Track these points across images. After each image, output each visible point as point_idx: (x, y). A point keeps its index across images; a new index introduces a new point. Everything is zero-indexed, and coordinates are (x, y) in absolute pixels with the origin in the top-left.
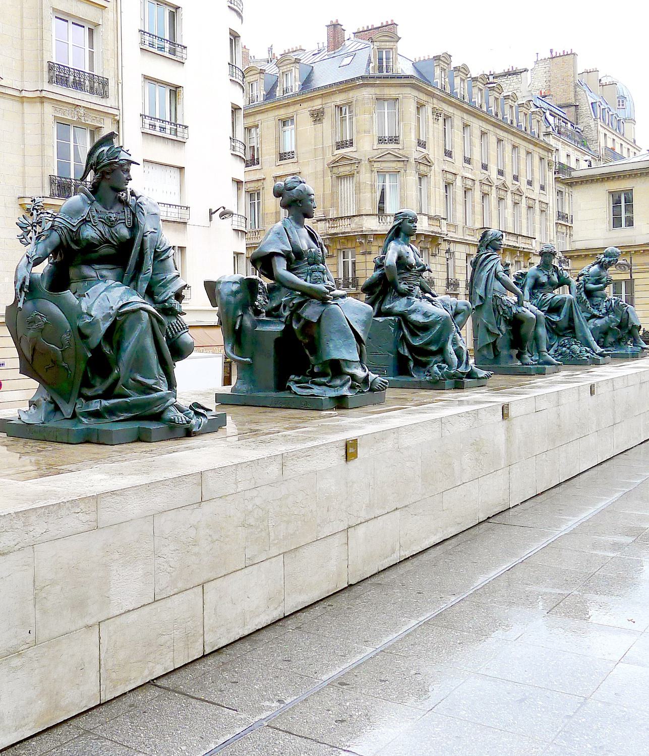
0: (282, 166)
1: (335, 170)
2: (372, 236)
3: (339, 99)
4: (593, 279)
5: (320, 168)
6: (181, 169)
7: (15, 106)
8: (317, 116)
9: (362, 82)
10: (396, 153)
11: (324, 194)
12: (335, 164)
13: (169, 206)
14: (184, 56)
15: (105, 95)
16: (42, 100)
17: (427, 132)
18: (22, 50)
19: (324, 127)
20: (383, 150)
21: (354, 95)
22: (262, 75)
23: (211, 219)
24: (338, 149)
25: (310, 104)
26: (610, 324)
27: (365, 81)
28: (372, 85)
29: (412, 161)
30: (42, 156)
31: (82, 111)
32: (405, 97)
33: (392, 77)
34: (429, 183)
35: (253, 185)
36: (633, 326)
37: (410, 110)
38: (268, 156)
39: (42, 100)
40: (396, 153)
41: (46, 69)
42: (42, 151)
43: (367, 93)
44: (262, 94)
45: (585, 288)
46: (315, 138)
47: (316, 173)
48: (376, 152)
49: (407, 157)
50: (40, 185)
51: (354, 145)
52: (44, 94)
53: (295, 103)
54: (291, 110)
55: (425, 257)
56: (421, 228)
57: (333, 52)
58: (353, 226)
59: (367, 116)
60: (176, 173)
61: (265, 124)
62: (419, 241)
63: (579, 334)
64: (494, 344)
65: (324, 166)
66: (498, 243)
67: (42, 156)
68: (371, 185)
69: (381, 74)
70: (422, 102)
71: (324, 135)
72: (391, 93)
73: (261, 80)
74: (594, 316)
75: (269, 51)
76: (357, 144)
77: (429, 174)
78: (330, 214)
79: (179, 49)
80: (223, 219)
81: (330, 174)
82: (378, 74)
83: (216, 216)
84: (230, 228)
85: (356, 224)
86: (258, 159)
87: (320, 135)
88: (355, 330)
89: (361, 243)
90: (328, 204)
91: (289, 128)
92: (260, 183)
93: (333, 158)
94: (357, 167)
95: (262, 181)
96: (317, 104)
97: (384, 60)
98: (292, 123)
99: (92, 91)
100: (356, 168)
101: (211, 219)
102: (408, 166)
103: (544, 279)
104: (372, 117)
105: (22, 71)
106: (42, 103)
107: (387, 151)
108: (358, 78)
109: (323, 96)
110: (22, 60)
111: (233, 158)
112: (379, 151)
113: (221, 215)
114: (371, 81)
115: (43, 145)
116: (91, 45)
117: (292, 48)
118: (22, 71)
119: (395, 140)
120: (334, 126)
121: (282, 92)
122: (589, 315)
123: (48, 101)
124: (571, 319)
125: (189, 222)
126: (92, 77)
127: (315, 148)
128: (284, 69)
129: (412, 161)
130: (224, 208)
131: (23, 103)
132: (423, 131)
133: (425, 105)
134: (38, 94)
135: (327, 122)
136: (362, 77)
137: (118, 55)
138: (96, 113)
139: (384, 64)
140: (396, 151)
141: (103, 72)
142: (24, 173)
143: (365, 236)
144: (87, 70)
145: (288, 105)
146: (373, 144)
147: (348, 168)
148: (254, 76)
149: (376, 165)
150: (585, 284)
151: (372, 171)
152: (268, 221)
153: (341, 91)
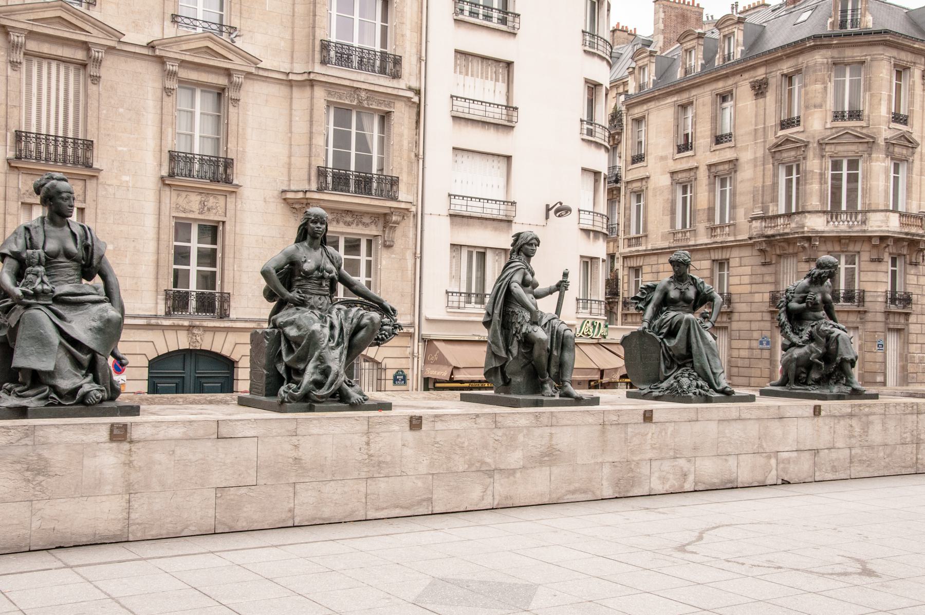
0: (717, 152)
1: (777, 156)
2: (818, 239)
3: (786, 67)
4: (797, 296)
5: (760, 153)
6: (509, 158)
7: (283, 91)
8: (760, 89)
9: (812, 44)
10: (857, 132)
11: (763, 187)
12: (776, 149)
13: (469, 199)
14: (517, 26)
15: (396, 76)
16: (312, 83)
17: (911, 103)
18: (293, 28)
19: (768, 103)
20: (839, 129)
21: (803, 60)
22: (700, 40)
23: (547, 217)
24: (782, 129)
25: (752, 73)
26: (810, 355)
27: (818, 42)
28: (828, 46)
29: (881, 142)
30: (310, 145)
31: (363, 94)
32: (876, 60)
33: (857, 34)
34: (910, 170)
35: (684, 175)
36: (842, 359)
37: (881, 75)
38: (703, 139)
39: (312, 83)
40: (857, 132)
41: (318, 48)
42: (311, 139)
43: (819, 58)
44: (700, 63)
45: (787, 306)
46: (756, 116)
47: (755, 159)
48: (828, 133)
49: (872, 137)
50: (306, 177)
51: (802, 123)
52: (312, 76)
53: (734, 74)
54: (730, 82)
55: (901, 266)
56: (887, 229)
57: (792, 6)
58: (793, 225)
59: (819, 87)
60: (503, 164)
61: (700, 101)
62: (885, 245)
63: (697, 364)
64: (502, 367)
65: (764, 150)
66: (529, 248)
67: (310, 145)
68: (821, 174)
69: (844, 31)
70: (902, 63)
71: (767, 112)
72: (855, 54)
73: (700, 47)
74: (793, 345)
75: (733, 8)
76: (804, 122)
77: (911, 159)
78: (770, 211)
79: (510, 18)
80: (559, 216)
81: (771, 161)
82: (838, 30)
83: (552, 213)
84: (576, 228)
85: (797, 223)
86: (692, 143)
87: (762, 112)
88: (69, 335)
89: (804, 248)
90: (768, 198)
91: (728, 104)
92: (692, 174)
93: (775, 141)
94: (804, 151)
95: (695, 171)
96: (760, 73)
97: (849, 12)
98: (732, 99)
99: (383, 71)
100: (802, 153)
101: (547, 217)
102: (874, 149)
103: (674, 294)
104: (825, 88)
105: (292, 52)
106: (312, 86)
107: (844, 129)
108: (809, 38)
109: (766, 63)
110: (293, 39)
111: (585, 145)
112: (834, 130)
113: (556, 212)
114: (826, 42)
115: (311, 133)
116: (385, 18)
117: (754, 4)
118: (292, 52)
119: (855, 115)
120: (779, 101)
121: (721, 60)
122: (788, 343)
123: (319, 84)
124: (689, 346)
125: (515, 220)
126: (384, 55)
127: (755, 130)
128: (726, 31)
129: (881, 142)
130: (561, 203)
131: (291, 86)
132: (905, 102)
133: (909, 68)
134: (305, 77)
135: (770, 97)
136: (815, 37)
137: (423, 29)
138: (383, 95)
139: (849, 17)
140: (858, 130)
141: (395, 50)
142: (290, 164)
143: (809, 239)
144: (378, 48)
145: (726, 76)
146: (826, 122)
147: (793, 153)
148: (691, 42)
149: (828, 148)
150: (787, 303)
151: (823, 156)
152: (699, 219)
153: (789, 56)
